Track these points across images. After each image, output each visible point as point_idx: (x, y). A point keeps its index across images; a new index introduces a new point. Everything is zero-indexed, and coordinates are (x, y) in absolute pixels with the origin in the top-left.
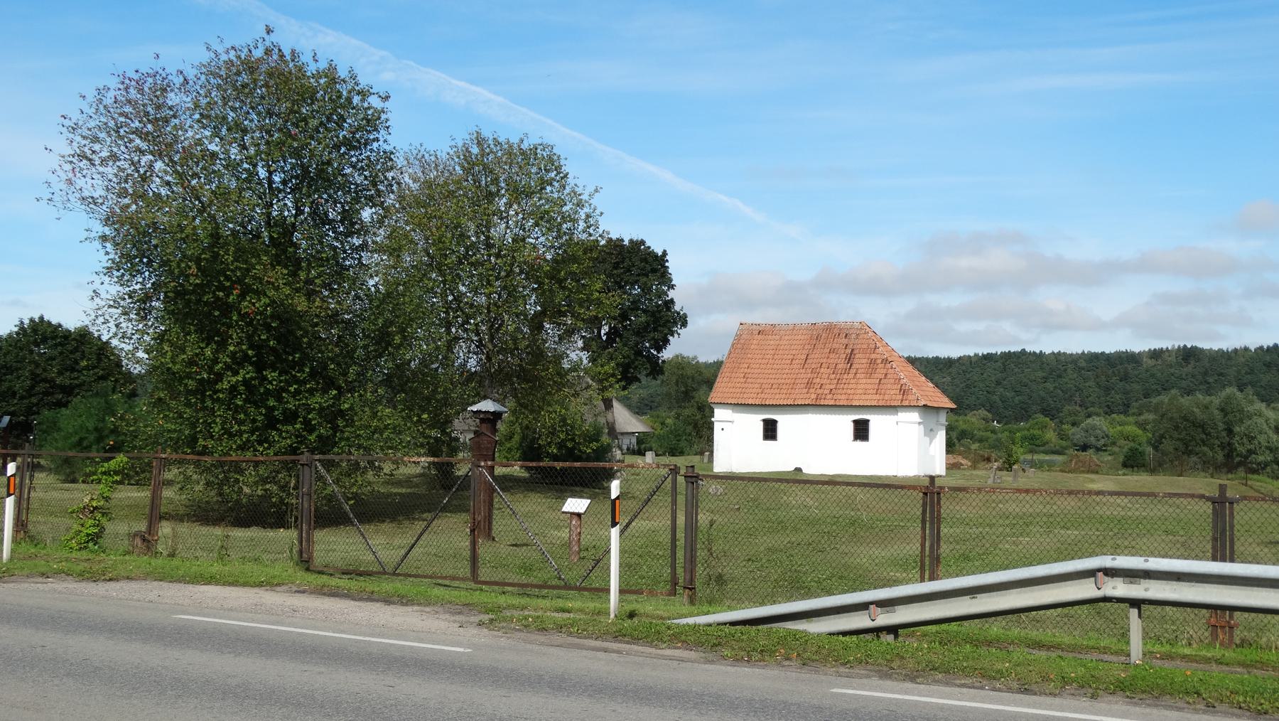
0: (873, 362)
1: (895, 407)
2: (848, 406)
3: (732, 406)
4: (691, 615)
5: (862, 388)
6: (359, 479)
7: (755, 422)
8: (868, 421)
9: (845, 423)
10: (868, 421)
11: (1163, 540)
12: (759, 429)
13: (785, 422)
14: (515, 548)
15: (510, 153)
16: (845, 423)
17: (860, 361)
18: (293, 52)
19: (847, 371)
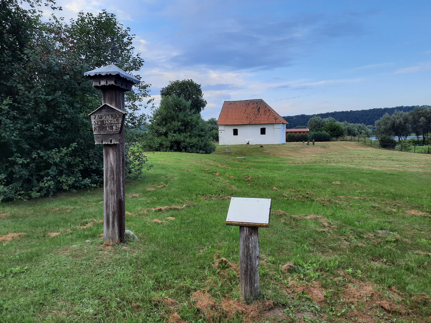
0: (265, 111)
1: (274, 124)
2: (260, 124)
3: (224, 126)
4: (107, 190)
5: (263, 118)
6: (363, 267)
7: (230, 131)
8: (265, 128)
9: (258, 130)
10: (265, 128)
11: (196, 190)
12: (232, 132)
13: (240, 130)
14: (277, 162)
15: (167, 89)
16: (258, 130)
17: (262, 111)
18: (128, 28)
19: (258, 114)
